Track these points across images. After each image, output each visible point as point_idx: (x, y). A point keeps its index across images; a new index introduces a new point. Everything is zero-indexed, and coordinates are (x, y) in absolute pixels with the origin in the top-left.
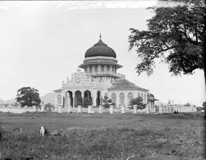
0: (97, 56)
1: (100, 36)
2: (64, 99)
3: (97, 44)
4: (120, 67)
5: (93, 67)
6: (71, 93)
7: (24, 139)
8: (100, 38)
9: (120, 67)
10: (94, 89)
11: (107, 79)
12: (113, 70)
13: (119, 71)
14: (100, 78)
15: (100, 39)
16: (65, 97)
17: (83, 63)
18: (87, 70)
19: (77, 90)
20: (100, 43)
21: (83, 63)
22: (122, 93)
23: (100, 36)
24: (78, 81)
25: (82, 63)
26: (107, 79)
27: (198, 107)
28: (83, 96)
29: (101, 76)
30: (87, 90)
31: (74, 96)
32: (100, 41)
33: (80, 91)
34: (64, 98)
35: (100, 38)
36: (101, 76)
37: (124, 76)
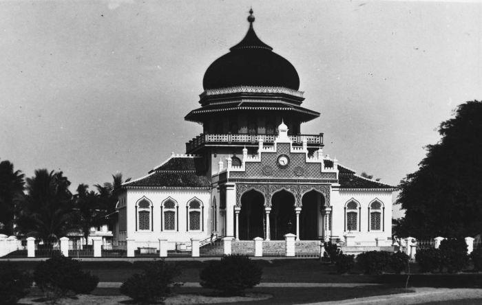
8: (251, 26)
21: (199, 106)
35: (251, 26)
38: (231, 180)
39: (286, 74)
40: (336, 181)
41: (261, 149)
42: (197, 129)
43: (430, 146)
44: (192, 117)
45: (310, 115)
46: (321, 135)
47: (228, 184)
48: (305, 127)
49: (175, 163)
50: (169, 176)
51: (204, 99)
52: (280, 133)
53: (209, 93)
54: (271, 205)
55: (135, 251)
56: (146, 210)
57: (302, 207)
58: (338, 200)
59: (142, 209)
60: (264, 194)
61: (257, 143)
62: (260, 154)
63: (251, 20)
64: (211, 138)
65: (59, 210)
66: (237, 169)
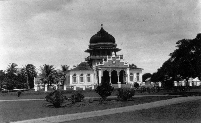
21: (89, 48)
23: (102, 25)
30: (122, 70)
37: (85, 59)
38: (100, 68)
39: (112, 40)
40: (128, 67)
41: (108, 59)
42: (88, 54)
43: (171, 54)
44: (87, 51)
45: (118, 50)
46: (123, 55)
47: (99, 69)
48: (117, 53)
49: (82, 64)
50: (82, 67)
51: (90, 47)
52: (113, 55)
53: (91, 45)
54: (111, 74)
55: (85, 59)
56: (89, 76)
57: (120, 75)
58: (128, 72)
59: (131, 75)
60: (109, 71)
61: (107, 58)
62: (103, 63)
63: (102, 25)
64: (92, 57)
65: (167, 75)
66: (101, 65)
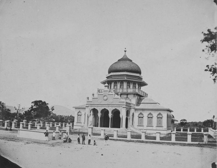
0: (136, 73)
1: (125, 51)
2: (88, 117)
3: (121, 59)
4: (144, 84)
5: (118, 83)
6: (95, 111)
7: (196, 124)
8: (125, 53)
9: (144, 84)
10: (124, 108)
11: (134, 97)
12: (138, 87)
13: (143, 88)
14: (125, 96)
15: (124, 54)
16: (89, 115)
17: (106, 79)
18: (111, 86)
19: (104, 108)
20: (125, 59)
22: (150, 114)
23: (125, 51)
24: (105, 98)
25: (105, 79)
26: (134, 97)
27: (204, 137)
28: (99, 115)
29: (127, 94)
31: (99, 115)
32: (125, 55)
33: (97, 110)
34: (88, 116)
35: (125, 53)
36: (127, 94)
